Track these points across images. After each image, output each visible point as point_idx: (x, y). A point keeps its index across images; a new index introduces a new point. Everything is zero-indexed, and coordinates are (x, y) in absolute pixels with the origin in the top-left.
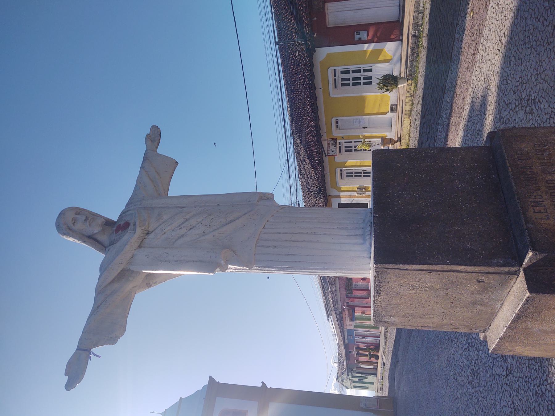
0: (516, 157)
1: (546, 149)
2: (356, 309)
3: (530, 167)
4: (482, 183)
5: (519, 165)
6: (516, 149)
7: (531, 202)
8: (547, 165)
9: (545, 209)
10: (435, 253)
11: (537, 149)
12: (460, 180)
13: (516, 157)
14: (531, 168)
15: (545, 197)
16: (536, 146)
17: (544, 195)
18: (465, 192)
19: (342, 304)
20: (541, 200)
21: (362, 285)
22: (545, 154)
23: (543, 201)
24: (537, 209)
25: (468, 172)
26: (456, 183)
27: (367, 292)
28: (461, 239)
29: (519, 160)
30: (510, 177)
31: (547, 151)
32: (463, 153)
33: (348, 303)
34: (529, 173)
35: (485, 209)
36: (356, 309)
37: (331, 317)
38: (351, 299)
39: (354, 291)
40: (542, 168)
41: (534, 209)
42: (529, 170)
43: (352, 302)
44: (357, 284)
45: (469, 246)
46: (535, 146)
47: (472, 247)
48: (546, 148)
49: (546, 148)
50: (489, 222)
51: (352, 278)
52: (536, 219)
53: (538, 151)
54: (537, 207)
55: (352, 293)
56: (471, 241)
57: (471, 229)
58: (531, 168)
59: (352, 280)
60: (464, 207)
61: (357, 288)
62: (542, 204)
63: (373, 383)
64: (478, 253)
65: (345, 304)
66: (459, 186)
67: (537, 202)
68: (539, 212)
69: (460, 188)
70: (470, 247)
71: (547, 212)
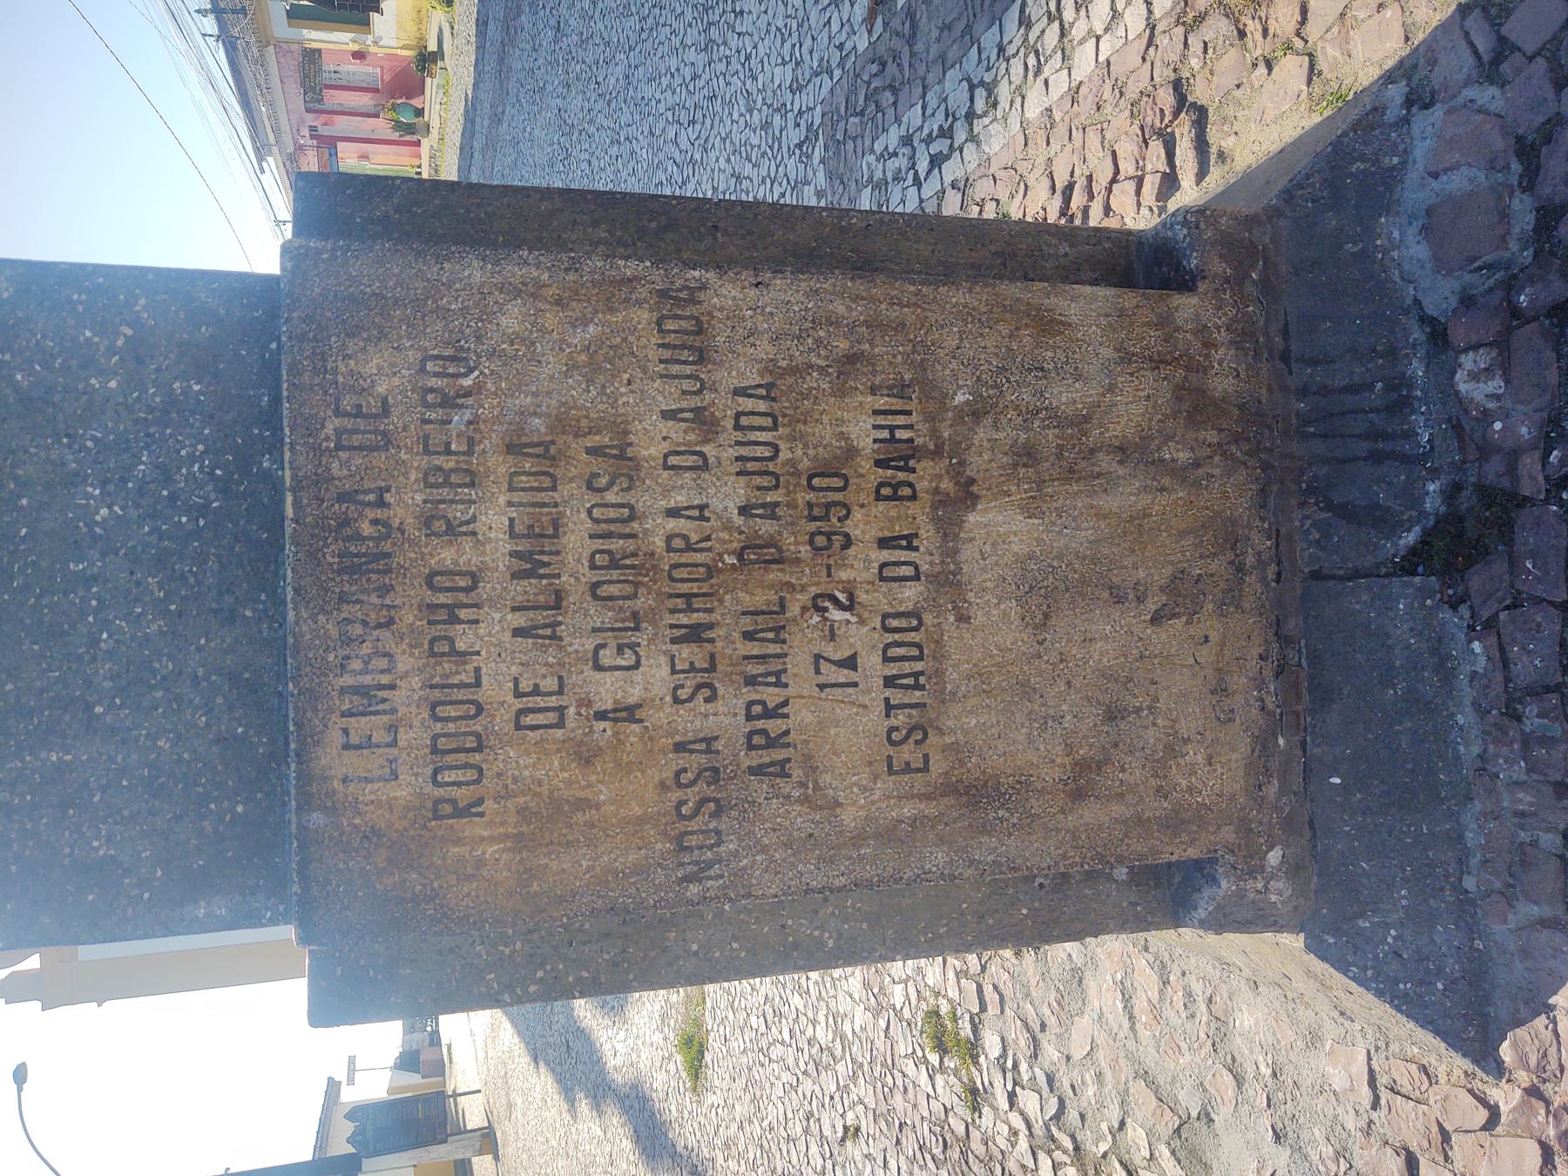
0: (329, 429)
1: (468, 394)
2: (340, 145)
3: (382, 491)
4: (206, 498)
5: (333, 478)
6: (340, 379)
7: (343, 691)
8: (451, 485)
9: (391, 726)
10: (214, 505)
11: (432, 390)
12: (104, 483)
13: (329, 429)
14: (381, 503)
15: (404, 663)
16: (430, 366)
17: (404, 653)
18: (123, 551)
19: (295, 132)
20: (385, 679)
21: (354, 73)
22: (456, 418)
23: (392, 687)
24: (360, 725)
25: (152, 430)
26: (88, 496)
27: (371, 95)
28: (71, 811)
29: (339, 447)
30: (284, 549)
31: (470, 401)
32: (146, 308)
33: (313, 129)
34: (366, 529)
35: (199, 649)
36: (340, 145)
37: (270, 159)
38: (324, 117)
39: (327, 93)
40: (425, 502)
41: (346, 731)
42: (370, 513)
43: (325, 124)
44: (338, 69)
45: (97, 849)
46: (422, 370)
47: (112, 852)
48: (467, 382)
49: (467, 382)
50: (204, 719)
51: (319, 51)
52: (345, 780)
53: (430, 398)
54: (363, 720)
55: (320, 101)
56: (110, 820)
57: (120, 757)
58: (381, 503)
59: (320, 56)
60: (105, 636)
61: (340, 83)
62: (385, 700)
63: (479, 1091)
64: (135, 881)
65: (306, 132)
66: (98, 518)
67: (362, 691)
68: (368, 744)
69: (98, 530)
70: (101, 852)
71: (394, 744)
